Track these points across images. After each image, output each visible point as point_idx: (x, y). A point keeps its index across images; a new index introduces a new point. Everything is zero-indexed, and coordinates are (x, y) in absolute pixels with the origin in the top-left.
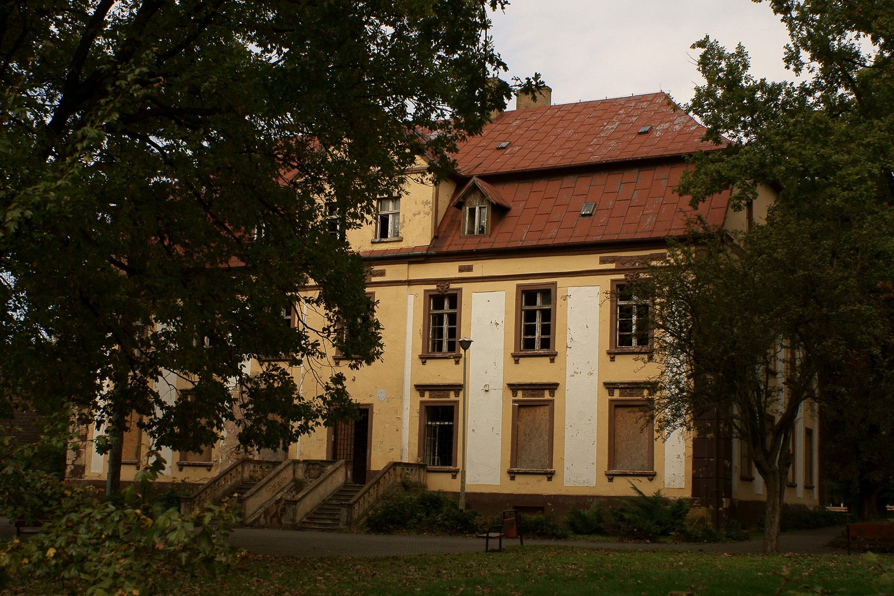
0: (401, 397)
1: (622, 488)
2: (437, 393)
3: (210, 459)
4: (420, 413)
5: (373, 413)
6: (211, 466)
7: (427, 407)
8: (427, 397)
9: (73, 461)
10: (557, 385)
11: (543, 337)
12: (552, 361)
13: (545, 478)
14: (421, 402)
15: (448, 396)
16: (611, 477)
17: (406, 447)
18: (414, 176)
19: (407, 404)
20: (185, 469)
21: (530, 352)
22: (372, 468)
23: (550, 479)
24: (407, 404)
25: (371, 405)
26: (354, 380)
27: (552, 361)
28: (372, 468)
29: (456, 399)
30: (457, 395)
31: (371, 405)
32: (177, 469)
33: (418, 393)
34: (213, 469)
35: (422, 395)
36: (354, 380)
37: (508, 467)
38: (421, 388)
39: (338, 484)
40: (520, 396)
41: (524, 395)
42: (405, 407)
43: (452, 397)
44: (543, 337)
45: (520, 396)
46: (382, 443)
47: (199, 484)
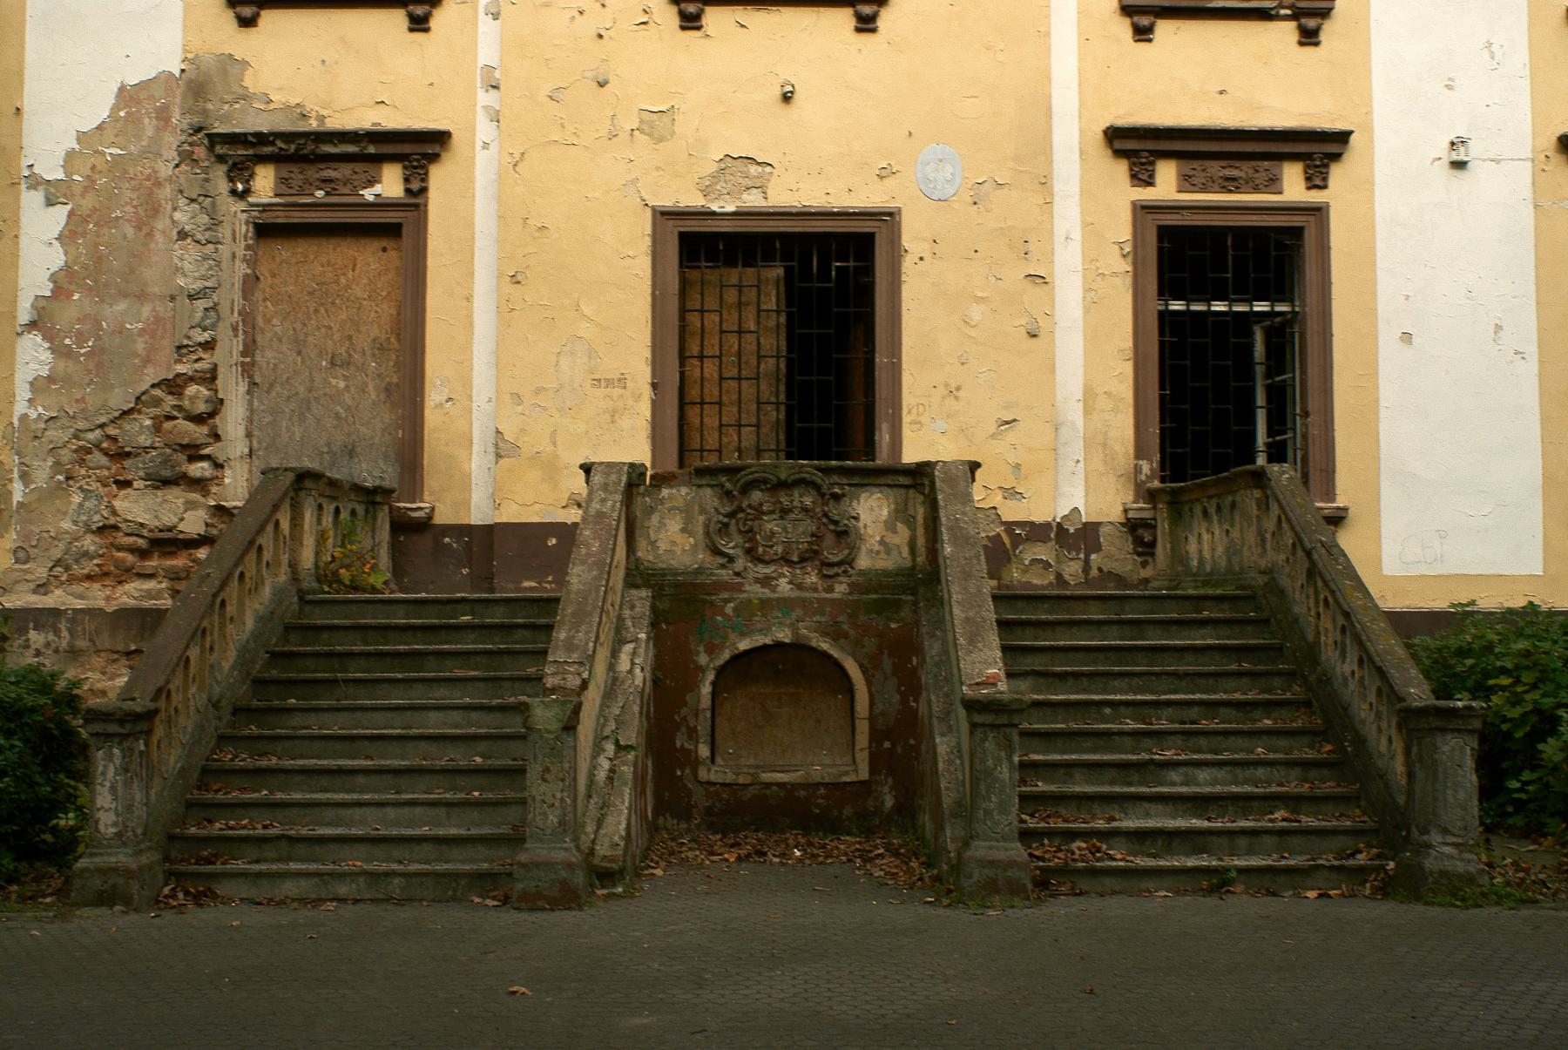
0: (1045, 183)
2: (1216, 169)
7: (1164, 233)
10: (1343, 137)
12: (1309, 37)
14: (1142, 210)
15: (1273, 184)
17: (1074, 414)
19: (1068, 215)
22: (1533, 564)
24: (1068, 215)
25: (888, 218)
26: (787, 98)
27: (1309, 37)
28: (1533, 564)
29: (1315, 197)
30: (1317, 178)
31: (888, 218)
33: (1121, 168)
35: (1142, 176)
36: (787, 98)
38: (1136, 146)
40: (1167, 184)
41: (1186, 182)
42: (1060, 227)
45: (1167, 184)
46: (953, 392)
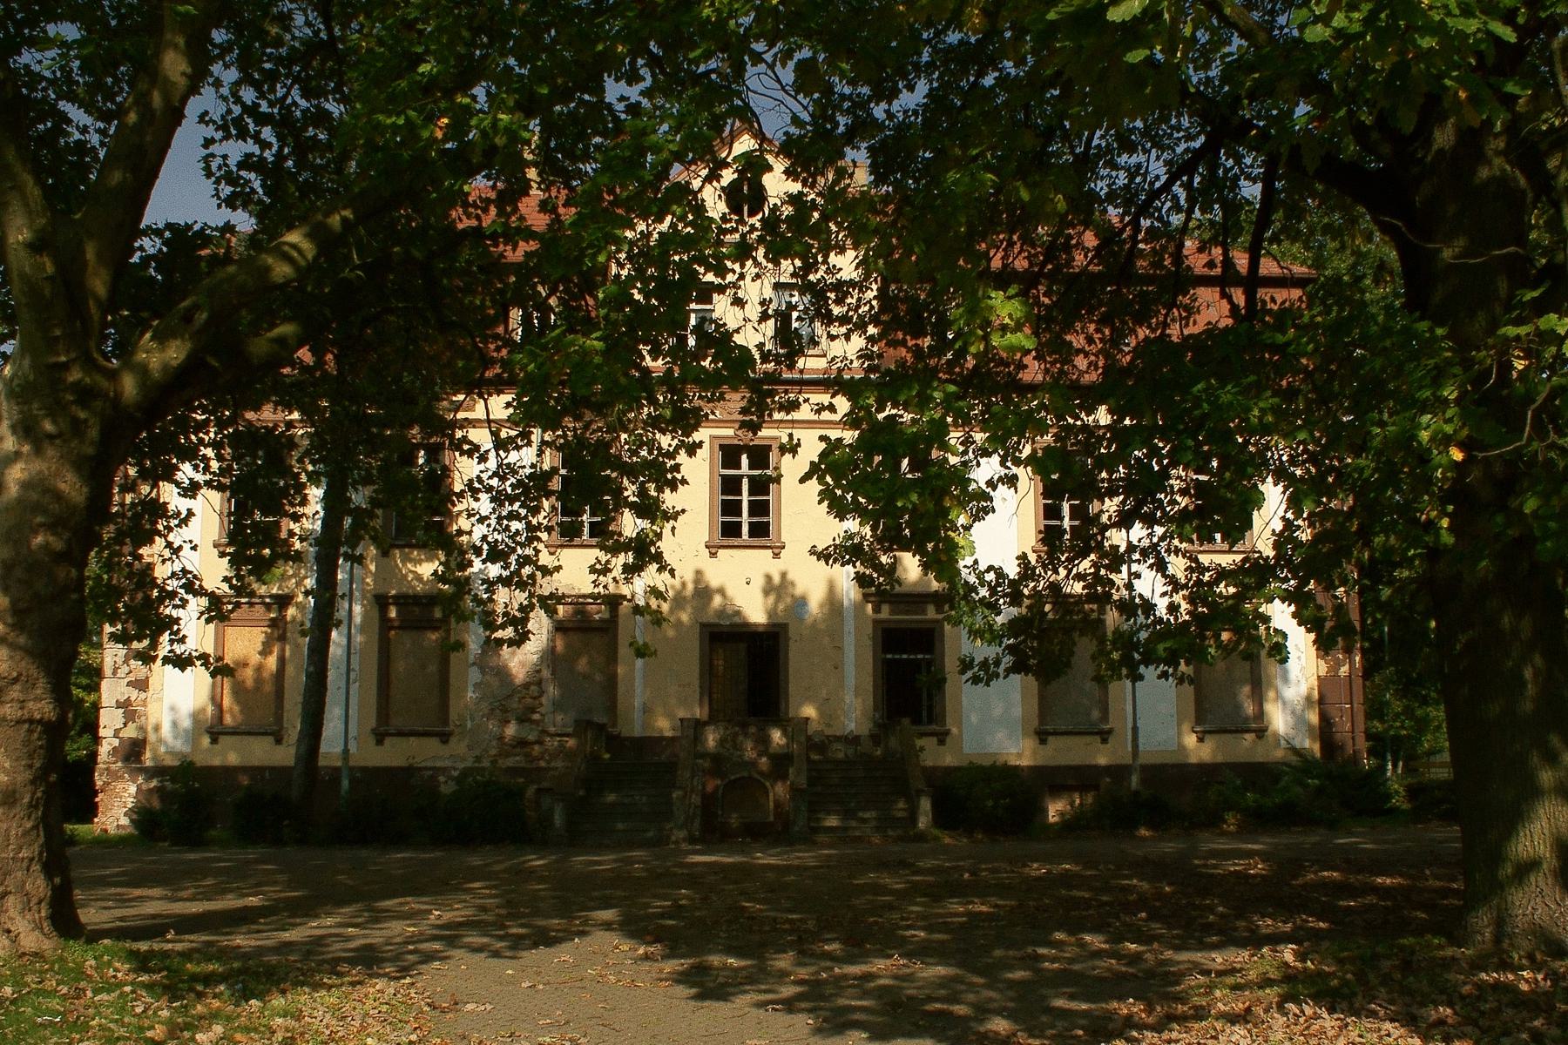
1: (393, 754)
3: (446, 722)
4: (874, 638)
5: (787, 639)
6: (450, 734)
8: (885, 613)
9: (117, 731)
11: (755, 520)
13: (1098, 738)
16: (1042, 736)
18: (1164, 179)
20: (388, 741)
21: (735, 542)
23: (1105, 741)
32: (372, 740)
34: (453, 740)
37: (373, 723)
39: (940, 763)
41: (892, 612)
43: (931, 613)
44: (755, 520)
47: (426, 768)
